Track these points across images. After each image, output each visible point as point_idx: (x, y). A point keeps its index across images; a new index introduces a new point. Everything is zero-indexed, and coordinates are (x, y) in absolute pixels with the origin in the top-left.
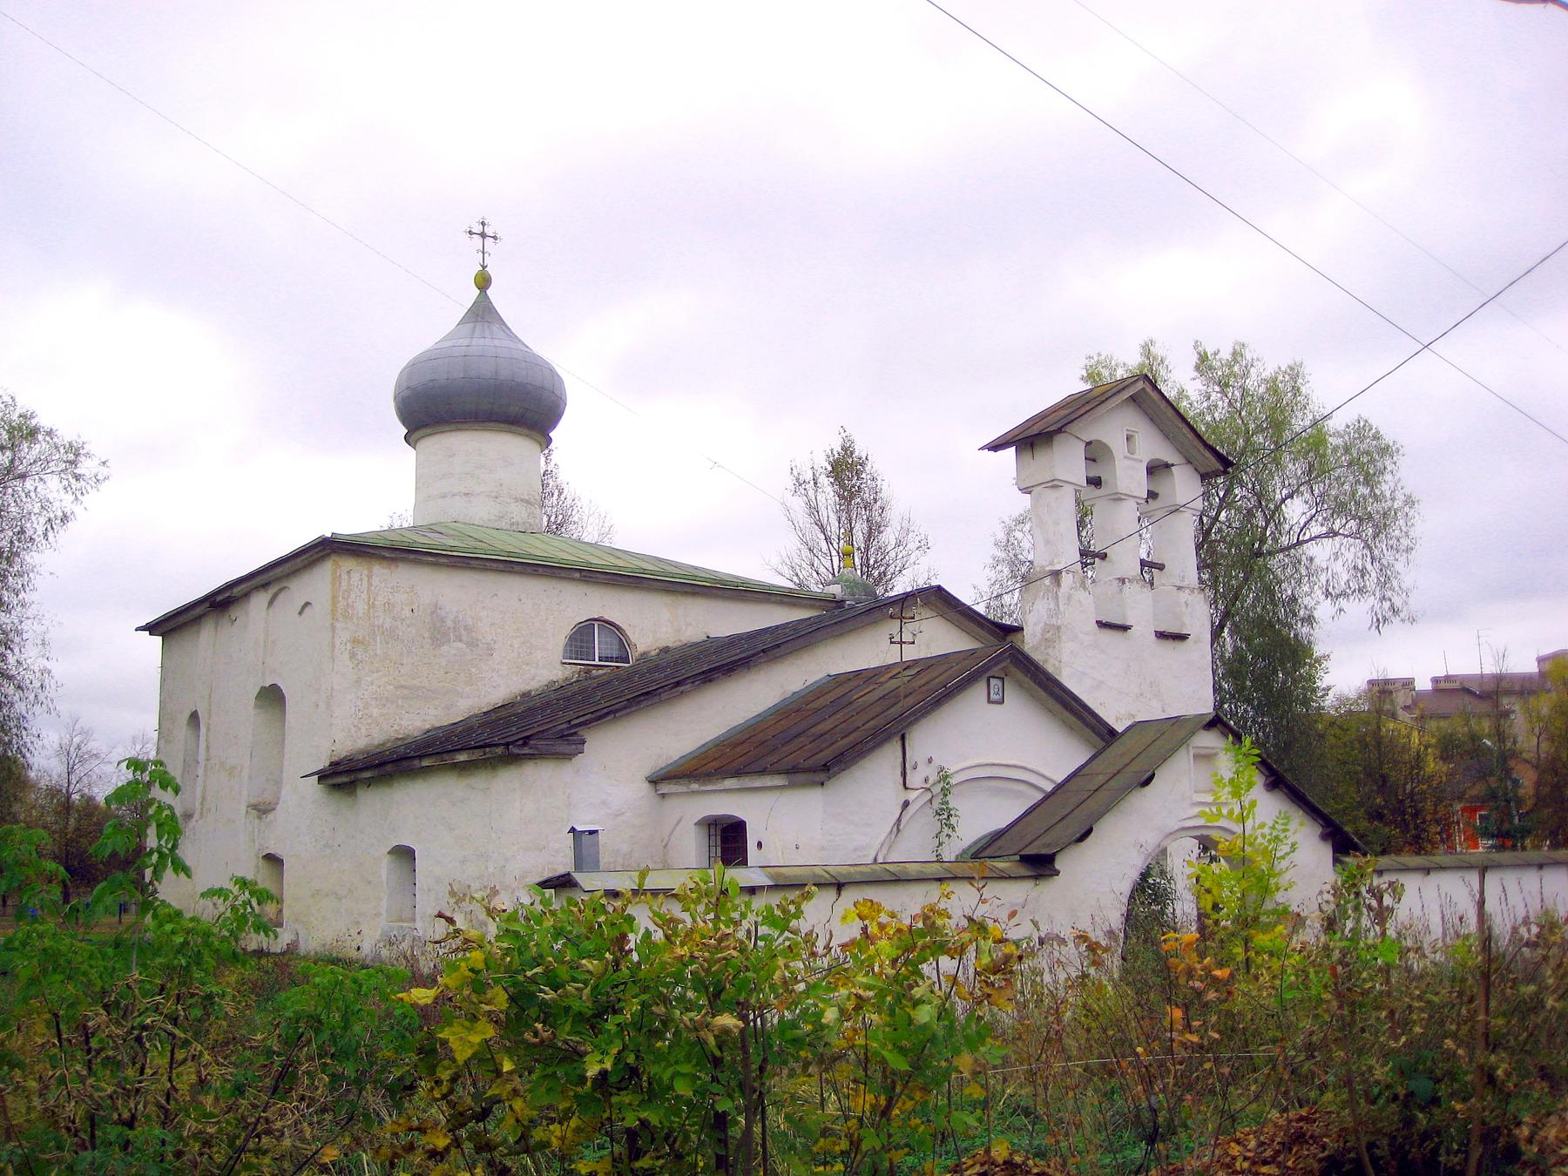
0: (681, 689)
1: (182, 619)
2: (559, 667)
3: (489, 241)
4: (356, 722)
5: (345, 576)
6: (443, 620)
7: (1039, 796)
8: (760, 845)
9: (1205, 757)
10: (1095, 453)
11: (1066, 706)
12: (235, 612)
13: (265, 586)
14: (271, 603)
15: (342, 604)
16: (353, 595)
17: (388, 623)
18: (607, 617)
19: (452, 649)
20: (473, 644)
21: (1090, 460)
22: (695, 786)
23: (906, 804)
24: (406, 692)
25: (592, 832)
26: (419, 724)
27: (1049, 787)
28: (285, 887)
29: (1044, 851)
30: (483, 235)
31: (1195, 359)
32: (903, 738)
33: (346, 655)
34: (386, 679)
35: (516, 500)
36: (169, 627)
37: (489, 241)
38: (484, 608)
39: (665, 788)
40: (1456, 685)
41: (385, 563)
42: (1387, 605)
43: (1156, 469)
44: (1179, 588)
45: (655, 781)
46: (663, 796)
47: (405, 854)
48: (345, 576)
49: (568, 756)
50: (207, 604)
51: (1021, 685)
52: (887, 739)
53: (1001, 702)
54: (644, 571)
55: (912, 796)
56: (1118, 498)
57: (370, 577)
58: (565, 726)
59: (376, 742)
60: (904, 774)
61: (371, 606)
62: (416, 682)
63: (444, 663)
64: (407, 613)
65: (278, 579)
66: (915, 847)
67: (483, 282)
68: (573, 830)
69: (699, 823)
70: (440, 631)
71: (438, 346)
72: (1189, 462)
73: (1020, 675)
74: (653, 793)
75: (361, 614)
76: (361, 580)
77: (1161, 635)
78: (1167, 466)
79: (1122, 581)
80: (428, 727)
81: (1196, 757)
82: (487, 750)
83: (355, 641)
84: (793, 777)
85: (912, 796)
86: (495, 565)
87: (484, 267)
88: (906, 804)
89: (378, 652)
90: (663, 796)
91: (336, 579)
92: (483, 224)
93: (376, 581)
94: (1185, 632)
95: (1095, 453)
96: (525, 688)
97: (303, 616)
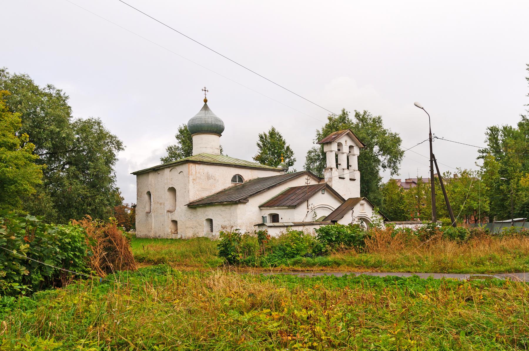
2: (231, 184)
3: (206, 92)
5: (191, 167)
7: (332, 211)
8: (282, 218)
9: (362, 205)
10: (340, 145)
11: (335, 194)
13: (169, 167)
14: (170, 171)
15: (190, 172)
18: (239, 174)
20: (215, 180)
21: (338, 146)
22: (268, 208)
23: (308, 212)
27: (334, 210)
29: (336, 220)
30: (205, 91)
31: (355, 114)
32: (308, 201)
35: (412, 272)
36: (139, 174)
37: (206, 92)
39: (262, 208)
40: (411, 181)
42: (394, 171)
43: (351, 147)
44: (354, 170)
45: (260, 207)
46: (261, 210)
47: (175, 222)
48: (191, 167)
49: (245, 203)
51: (327, 191)
52: (305, 201)
53: (324, 194)
54: (246, 165)
55: (309, 210)
56: (343, 153)
57: (195, 167)
60: (308, 206)
61: (196, 173)
62: (205, 187)
64: (202, 174)
65: (173, 166)
66: (309, 220)
67: (206, 101)
68: (263, 217)
69: (268, 215)
70: (208, 178)
71: (196, 116)
72: (357, 145)
73: (327, 189)
74: (259, 209)
77: (351, 179)
78: (353, 147)
79: (344, 169)
81: (361, 204)
85: (309, 210)
86: (218, 164)
88: (308, 212)
90: (261, 210)
91: (189, 166)
92: (205, 88)
93: (196, 168)
94: (355, 179)
95: (340, 145)
96: (224, 188)
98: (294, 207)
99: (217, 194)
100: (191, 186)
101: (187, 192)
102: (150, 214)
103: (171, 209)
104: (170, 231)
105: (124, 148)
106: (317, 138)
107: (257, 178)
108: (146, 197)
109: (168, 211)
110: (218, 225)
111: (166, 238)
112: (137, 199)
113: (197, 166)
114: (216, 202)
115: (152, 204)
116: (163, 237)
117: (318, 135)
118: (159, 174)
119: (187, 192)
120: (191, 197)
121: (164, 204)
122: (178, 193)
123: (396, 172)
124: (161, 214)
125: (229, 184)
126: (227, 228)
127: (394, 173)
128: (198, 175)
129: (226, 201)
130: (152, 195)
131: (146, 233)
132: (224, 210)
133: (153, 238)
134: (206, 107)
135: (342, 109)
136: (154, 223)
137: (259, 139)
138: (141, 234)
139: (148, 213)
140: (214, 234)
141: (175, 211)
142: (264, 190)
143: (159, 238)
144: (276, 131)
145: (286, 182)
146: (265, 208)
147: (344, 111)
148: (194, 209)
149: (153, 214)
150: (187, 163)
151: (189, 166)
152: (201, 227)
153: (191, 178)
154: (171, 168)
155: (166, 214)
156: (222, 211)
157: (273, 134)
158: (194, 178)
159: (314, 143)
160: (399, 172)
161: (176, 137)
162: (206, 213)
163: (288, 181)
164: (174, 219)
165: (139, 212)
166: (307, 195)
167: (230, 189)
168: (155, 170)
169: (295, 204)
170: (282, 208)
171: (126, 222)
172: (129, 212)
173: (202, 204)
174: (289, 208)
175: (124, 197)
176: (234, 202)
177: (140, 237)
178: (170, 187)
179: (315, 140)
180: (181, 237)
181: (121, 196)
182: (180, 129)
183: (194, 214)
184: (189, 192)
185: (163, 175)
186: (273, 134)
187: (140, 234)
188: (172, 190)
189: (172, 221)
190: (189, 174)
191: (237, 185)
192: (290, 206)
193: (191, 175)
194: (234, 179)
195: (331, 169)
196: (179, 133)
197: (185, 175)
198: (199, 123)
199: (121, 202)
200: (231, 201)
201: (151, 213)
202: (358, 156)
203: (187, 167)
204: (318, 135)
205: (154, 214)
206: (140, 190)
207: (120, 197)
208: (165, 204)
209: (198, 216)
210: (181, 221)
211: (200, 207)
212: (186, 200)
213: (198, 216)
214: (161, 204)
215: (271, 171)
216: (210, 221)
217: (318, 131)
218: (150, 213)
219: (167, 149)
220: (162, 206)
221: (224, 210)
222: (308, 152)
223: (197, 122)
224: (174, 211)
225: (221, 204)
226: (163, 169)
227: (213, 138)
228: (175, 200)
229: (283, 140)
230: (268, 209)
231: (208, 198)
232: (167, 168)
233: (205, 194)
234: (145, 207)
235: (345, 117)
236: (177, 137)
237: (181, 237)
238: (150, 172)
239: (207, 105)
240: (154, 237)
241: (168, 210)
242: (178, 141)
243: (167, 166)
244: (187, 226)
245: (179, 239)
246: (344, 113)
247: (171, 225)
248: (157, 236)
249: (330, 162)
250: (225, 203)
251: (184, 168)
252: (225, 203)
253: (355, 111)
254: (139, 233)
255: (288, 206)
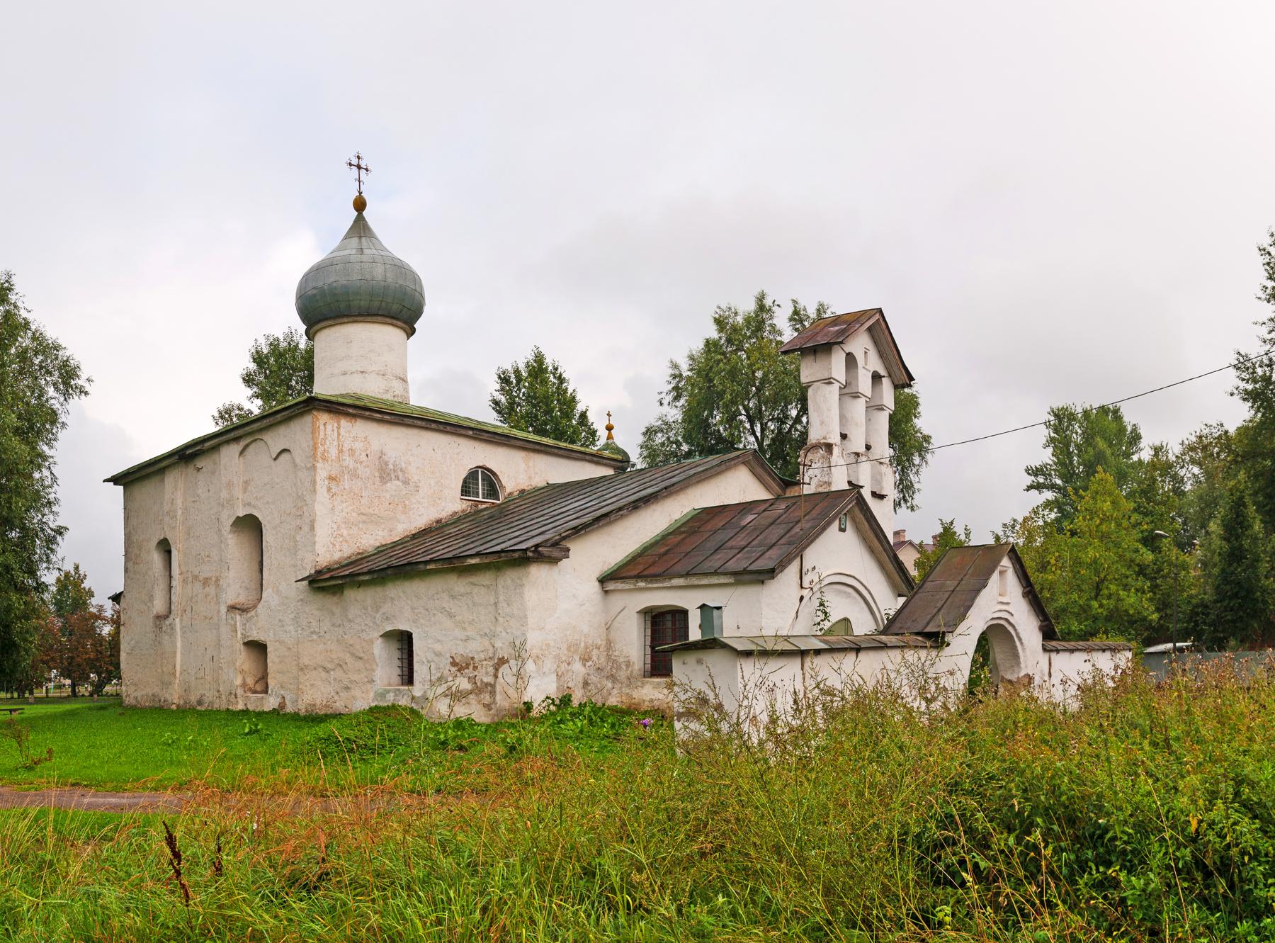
0: (621, 513)
1: (143, 473)
4: (332, 540)
5: (322, 427)
6: (386, 464)
10: (851, 360)
12: (200, 463)
13: (236, 439)
14: (241, 453)
15: (320, 449)
16: (328, 443)
17: (352, 465)
19: (393, 485)
20: (406, 483)
22: (642, 584)
23: (802, 598)
24: (364, 518)
25: (719, 608)
26: (372, 542)
28: (270, 664)
30: (359, 167)
31: (790, 311)
33: (325, 489)
34: (351, 508)
36: (128, 479)
38: (412, 455)
39: (611, 586)
41: (348, 419)
45: (603, 580)
47: (258, 648)
48: (322, 427)
49: (554, 561)
50: (177, 457)
55: (806, 593)
57: (339, 428)
58: (557, 537)
59: (346, 555)
60: (801, 578)
61: (341, 451)
62: (371, 511)
63: (388, 497)
64: (363, 457)
67: (360, 205)
70: (386, 472)
75: (333, 458)
76: (333, 430)
80: (378, 544)
82: (503, 555)
83: (331, 478)
84: (739, 577)
87: (360, 193)
88: (802, 598)
89: (346, 487)
90: (606, 592)
92: (359, 158)
94: (884, 493)
96: (438, 516)
97: (277, 461)
98: (766, 575)
99: (414, 536)
100: (322, 504)
101: (306, 528)
102: (168, 622)
103: (242, 598)
104: (238, 681)
105: (87, 388)
106: (670, 387)
107: (543, 484)
108: (156, 558)
109: (232, 608)
110: (438, 654)
111: (224, 707)
112: (126, 570)
113: (344, 423)
114: (431, 561)
115: (174, 583)
116: (212, 703)
117: (674, 376)
118: (199, 470)
119: (306, 528)
120: (320, 549)
121: (218, 580)
122: (268, 537)
123: (906, 501)
124: (206, 618)
125: (452, 504)
126: (475, 668)
127: (900, 504)
128: (348, 461)
129: (478, 554)
130: (174, 553)
131: (156, 690)
132: (462, 590)
133: (178, 706)
134: (360, 228)
135: (756, 292)
136: (182, 654)
137: (498, 387)
138: (139, 694)
139: (160, 618)
140: (417, 690)
141: (260, 606)
142: (620, 509)
143: (199, 708)
144: (549, 362)
145: (687, 487)
146: (627, 586)
147: (761, 299)
148: (334, 594)
149: (177, 620)
150: (309, 412)
151: (313, 424)
152: (359, 664)
153: (322, 472)
154: (243, 443)
155: (224, 617)
156: (453, 597)
157: (538, 369)
158: (334, 474)
159: (661, 404)
160: (918, 499)
161: (244, 379)
162: (387, 608)
163: (694, 479)
164: (255, 635)
165: (130, 618)
166: (797, 529)
167: (457, 519)
168: (188, 455)
169: (764, 563)
170: (705, 581)
171: (97, 660)
172: (107, 630)
173: (369, 572)
174: (738, 583)
175: (92, 589)
176: (516, 555)
177: (134, 702)
178: (241, 515)
179: (663, 395)
180: (282, 706)
181: (86, 585)
182: (257, 352)
183: (333, 614)
184: (312, 528)
185: (213, 473)
186: (538, 369)
187: (135, 694)
188: (250, 526)
189: (246, 644)
190: (314, 456)
191: (481, 507)
192: (745, 572)
193: (324, 459)
194: (467, 487)
195: (829, 447)
196: (253, 366)
197: (298, 461)
198: (343, 281)
199: (85, 603)
200: (502, 551)
201: (172, 616)
202: (890, 415)
203: (309, 430)
204: (674, 376)
205: (181, 620)
206: (134, 538)
207: (84, 588)
208: (221, 583)
209: (350, 621)
210: (281, 642)
211: (360, 585)
212: (302, 560)
213: (350, 621)
214: (206, 582)
215: (590, 461)
216: (404, 641)
217: (675, 366)
218: (166, 617)
219: (217, 415)
220: (211, 590)
221: (462, 590)
222: (644, 430)
223: (333, 279)
224: (255, 607)
225: (455, 566)
226: (215, 448)
227: (383, 335)
228: (256, 567)
229: (570, 391)
230: (641, 589)
231: (381, 550)
232: (228, 442)
233: (371, 538)
234: (151, 598)
235: (763, 322)
236: (248, 380)
237: (282, 706)
238: (168, 467)
239: (364, 219)
240: (182, 702)
241: (230, 602)
242: (249, 392)
243: (232, 435)
244: (305, 660)
245: (274, 711)
246: (762, 307)
247: (243, 659)
248: (193, 699)
249: (822, 423)
250: (473, 561)
251: (294, 435)
252: (473, 561)
253: (794, 301)
254: (131, 690)
255: (734, 574)
